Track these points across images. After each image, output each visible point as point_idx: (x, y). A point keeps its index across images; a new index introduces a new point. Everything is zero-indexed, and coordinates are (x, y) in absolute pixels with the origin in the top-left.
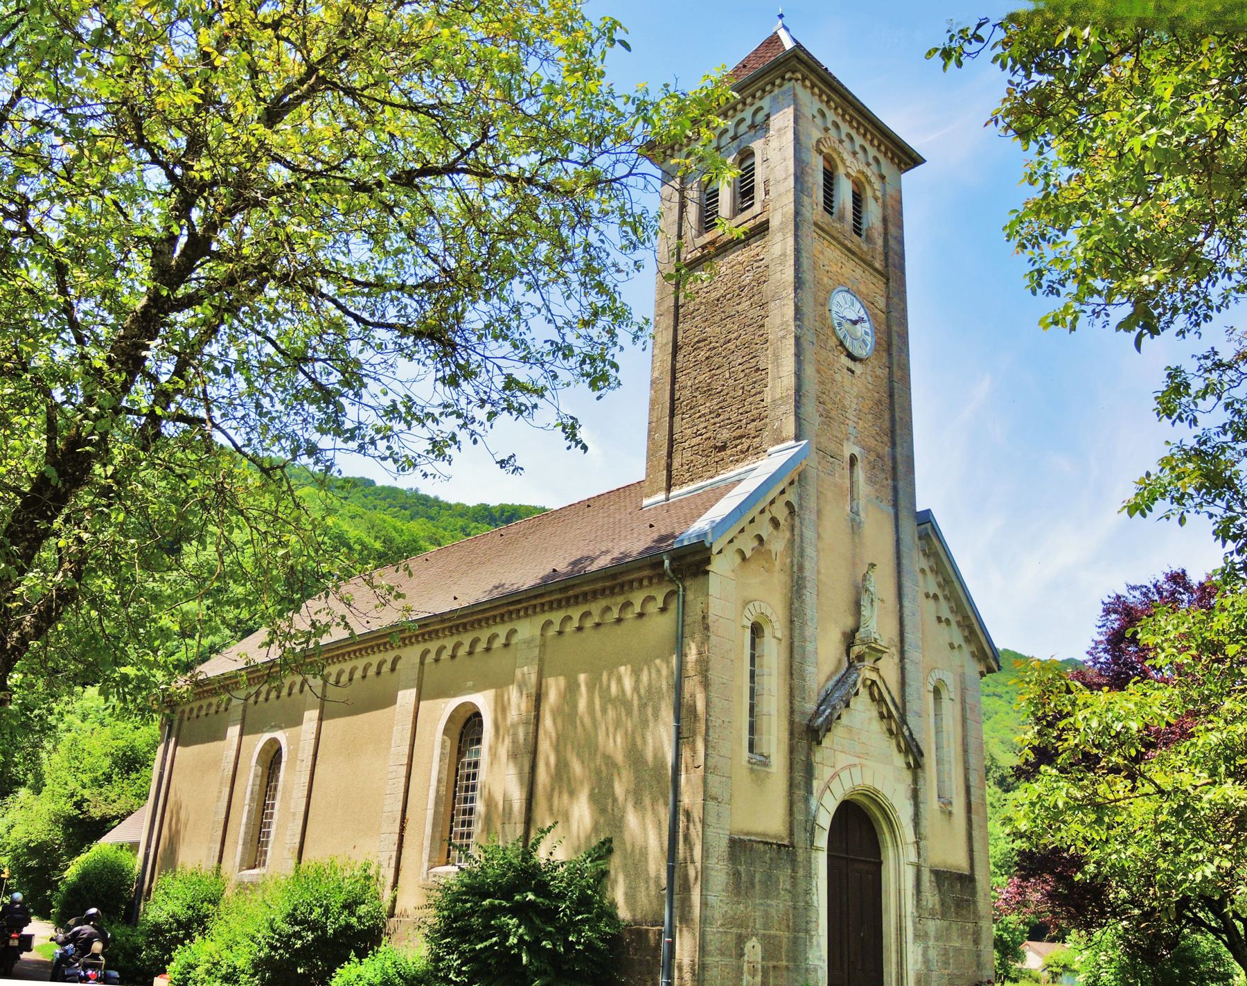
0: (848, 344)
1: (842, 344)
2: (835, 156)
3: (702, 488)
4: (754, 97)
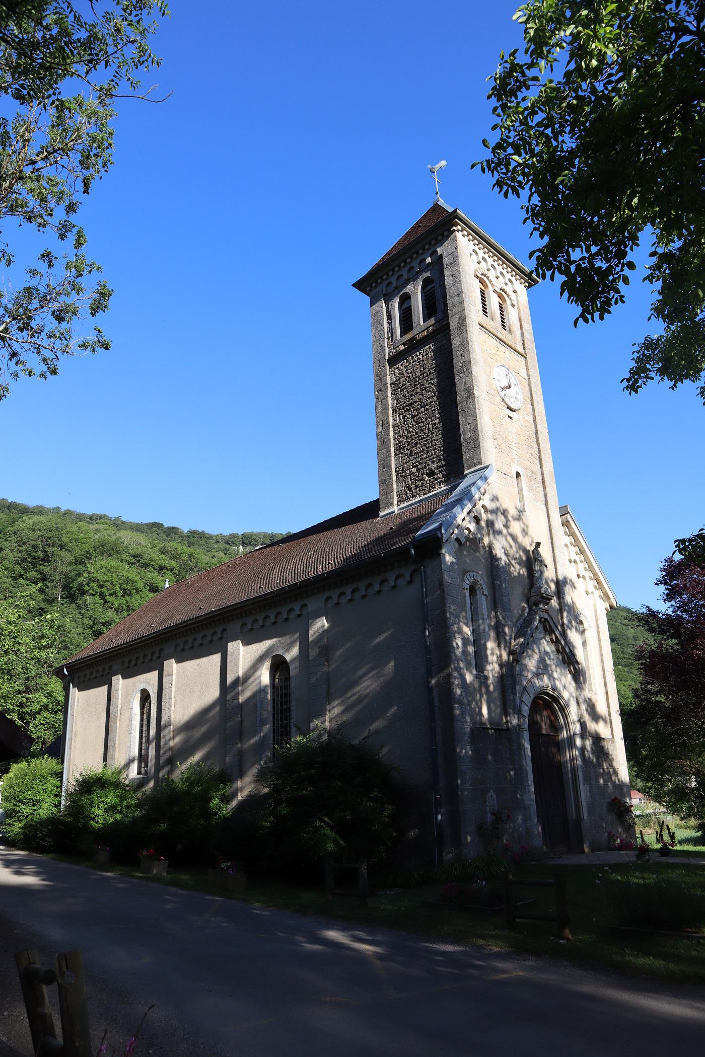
0: (507, 400)
1: (503, 400)
2: (485, 279)
3: (411, 505)
4: (430, 244)
